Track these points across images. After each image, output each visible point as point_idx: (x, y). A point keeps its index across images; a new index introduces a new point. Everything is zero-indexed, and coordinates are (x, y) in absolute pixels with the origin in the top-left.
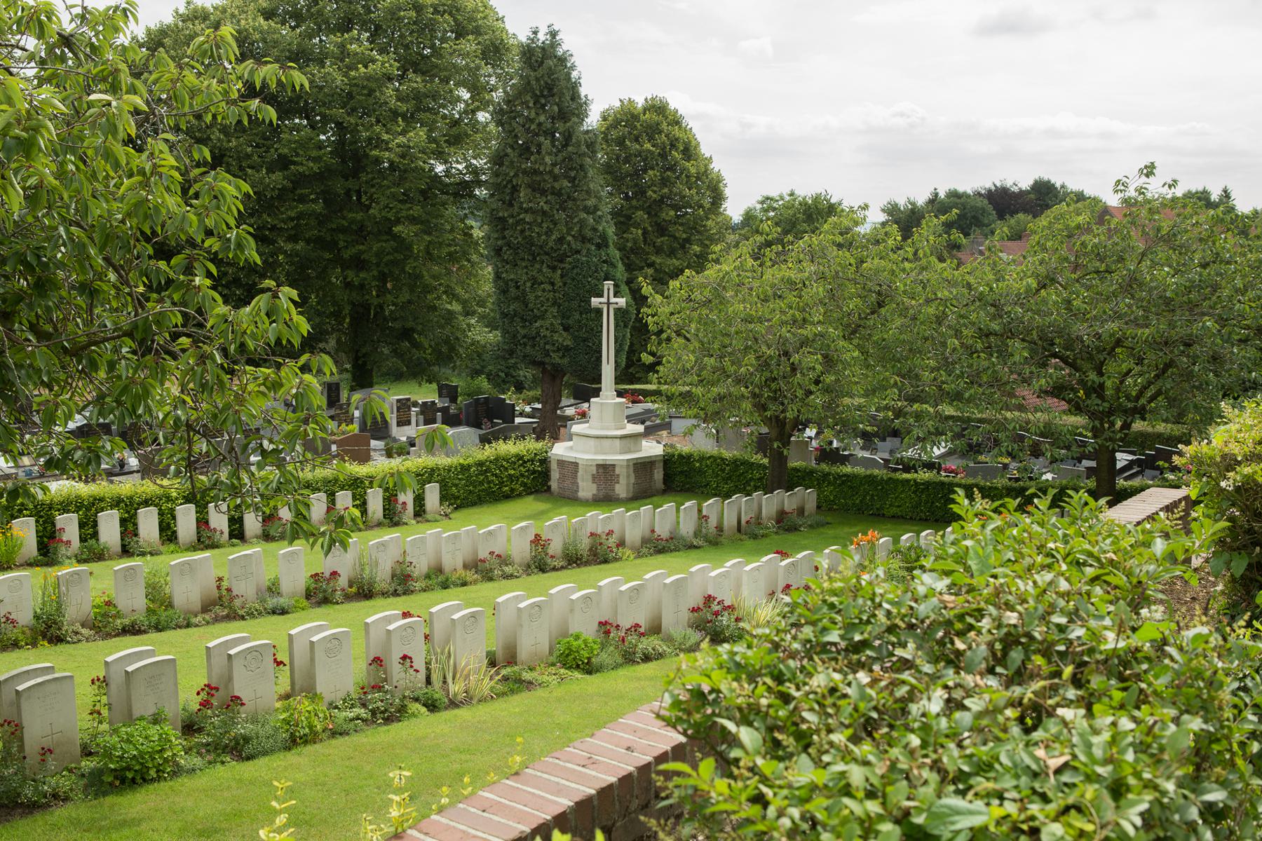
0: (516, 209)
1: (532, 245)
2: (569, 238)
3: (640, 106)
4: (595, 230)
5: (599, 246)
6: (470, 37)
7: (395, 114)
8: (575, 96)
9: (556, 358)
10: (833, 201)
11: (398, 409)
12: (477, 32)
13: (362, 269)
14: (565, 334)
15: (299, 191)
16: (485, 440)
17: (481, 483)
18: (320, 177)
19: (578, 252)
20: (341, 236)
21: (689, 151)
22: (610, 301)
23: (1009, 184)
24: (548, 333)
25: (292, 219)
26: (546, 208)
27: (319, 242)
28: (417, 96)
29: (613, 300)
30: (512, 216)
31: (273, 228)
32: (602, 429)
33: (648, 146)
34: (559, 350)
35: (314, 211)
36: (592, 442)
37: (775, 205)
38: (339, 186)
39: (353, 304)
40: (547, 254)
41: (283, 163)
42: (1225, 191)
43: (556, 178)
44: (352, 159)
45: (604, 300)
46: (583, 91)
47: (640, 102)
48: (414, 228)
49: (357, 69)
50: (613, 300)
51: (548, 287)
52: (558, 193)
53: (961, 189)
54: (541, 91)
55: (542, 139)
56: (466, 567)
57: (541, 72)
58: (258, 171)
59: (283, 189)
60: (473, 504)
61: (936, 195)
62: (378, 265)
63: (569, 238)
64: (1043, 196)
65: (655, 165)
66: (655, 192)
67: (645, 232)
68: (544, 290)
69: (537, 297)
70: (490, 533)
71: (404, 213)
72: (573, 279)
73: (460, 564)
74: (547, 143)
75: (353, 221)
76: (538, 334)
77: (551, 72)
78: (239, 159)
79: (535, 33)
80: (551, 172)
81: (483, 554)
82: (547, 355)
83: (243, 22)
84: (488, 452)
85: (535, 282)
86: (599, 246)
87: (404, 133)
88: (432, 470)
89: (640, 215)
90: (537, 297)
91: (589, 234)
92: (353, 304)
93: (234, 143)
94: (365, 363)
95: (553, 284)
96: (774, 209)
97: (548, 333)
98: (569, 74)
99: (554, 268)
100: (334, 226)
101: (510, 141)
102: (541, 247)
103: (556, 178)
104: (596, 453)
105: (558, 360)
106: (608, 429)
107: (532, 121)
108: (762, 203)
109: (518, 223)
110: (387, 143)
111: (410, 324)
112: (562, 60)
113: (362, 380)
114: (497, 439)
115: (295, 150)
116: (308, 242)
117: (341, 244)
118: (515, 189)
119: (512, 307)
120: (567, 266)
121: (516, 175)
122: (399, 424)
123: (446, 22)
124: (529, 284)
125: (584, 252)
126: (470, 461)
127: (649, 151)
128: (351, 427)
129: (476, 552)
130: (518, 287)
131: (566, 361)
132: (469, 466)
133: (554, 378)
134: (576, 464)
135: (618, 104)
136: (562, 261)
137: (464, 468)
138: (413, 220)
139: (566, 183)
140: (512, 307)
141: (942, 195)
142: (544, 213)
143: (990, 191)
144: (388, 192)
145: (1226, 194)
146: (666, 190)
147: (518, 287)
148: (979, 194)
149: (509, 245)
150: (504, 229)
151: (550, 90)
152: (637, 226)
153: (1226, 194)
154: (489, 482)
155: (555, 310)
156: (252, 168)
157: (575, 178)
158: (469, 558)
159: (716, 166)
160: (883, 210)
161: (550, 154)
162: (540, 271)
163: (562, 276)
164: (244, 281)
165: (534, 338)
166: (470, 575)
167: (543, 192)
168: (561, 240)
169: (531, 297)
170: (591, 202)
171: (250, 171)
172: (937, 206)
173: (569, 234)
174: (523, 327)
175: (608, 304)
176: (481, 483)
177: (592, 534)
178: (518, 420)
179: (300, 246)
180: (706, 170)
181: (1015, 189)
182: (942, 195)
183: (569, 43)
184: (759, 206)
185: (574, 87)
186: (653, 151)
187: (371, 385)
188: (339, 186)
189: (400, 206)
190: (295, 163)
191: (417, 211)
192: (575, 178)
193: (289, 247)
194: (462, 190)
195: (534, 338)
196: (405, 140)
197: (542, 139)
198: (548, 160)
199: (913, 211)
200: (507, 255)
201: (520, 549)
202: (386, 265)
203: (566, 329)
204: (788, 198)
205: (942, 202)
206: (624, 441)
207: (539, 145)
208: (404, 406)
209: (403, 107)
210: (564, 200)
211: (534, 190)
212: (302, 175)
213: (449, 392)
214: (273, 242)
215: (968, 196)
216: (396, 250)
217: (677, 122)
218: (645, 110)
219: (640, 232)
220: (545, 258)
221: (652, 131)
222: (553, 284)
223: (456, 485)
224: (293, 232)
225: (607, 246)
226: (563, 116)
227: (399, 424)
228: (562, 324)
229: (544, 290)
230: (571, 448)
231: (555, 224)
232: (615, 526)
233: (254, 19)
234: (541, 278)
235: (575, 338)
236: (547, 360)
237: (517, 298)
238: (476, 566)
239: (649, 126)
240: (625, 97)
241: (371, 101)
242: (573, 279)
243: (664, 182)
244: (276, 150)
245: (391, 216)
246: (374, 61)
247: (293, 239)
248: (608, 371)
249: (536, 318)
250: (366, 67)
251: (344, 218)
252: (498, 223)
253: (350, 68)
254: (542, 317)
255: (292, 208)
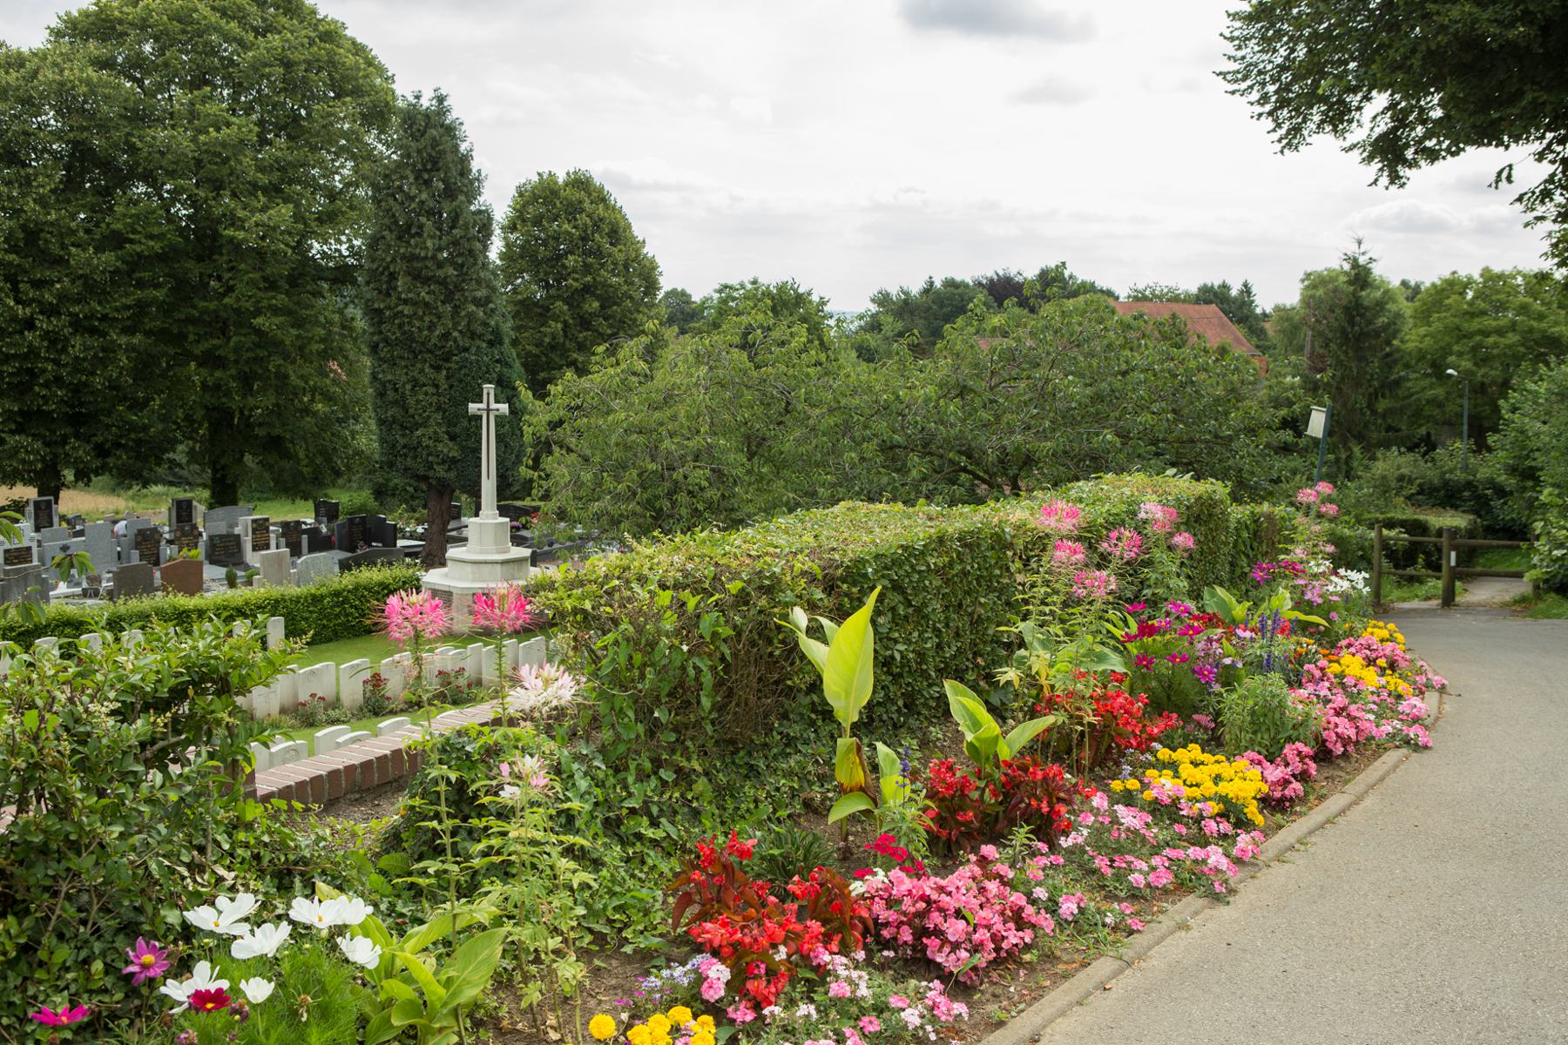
0: (394, 300)
1: (413, 340)
2: (455, 334)
3: (561, 181)
4: (486, 324)
5: (491, 344)
6: (348, 99)
7: (255, 186)
8: (464, 170)
9: (441, 471)
10: (801, 291)
11: (254, 530)
12: (357, 92)
13: (218, 368)
14: (451, 444)
15: (137, 275)
16: (345, 566)
17: (337, 616)
18: (162, 258)
19: (466, 350)
20: (191, 328)
21: (617, 231)
22: (489, 407)
23: (1012, 272)
24: (431, 443)
25: (128, 307)
26: (427, 298)
27: (163, 335)
28: (282, 167)
29: (494, 406)
30: (389, 308)
31: (104, 318)
32: (481, 552)
33: (566, 226)
34: (444, 462)
35: (155, 299)
36: (469, 568)
37: (735, 294)
38: (193, 269)
39: (206, 407)
40: (430, 351)
41: (116, 241)
42: (1245, 285)
43: (440, 265)
44: (206, 239)
45: (483, 406)
46: (475, 166)
47: (561, 178)
48: (277, 320)
49: (208, 133)
50: (494, 406)
51: (431, 390)
52: (443, 282)
53: (958, 279)
54: (424, 165)
55: (423, 219)
56: (283, 711)
57: (423, 142)
58: (84, 250)
59: (116, 272)
60: (329, 640)
61: (932, 283)
62: (236, 362)
63: (455, 334)
64: (1053, 282)
65: (580, 253)
66: (576, 280)
67: (566, 325)
68: (426, 394)
69: (418, 401)
70: (312, 672)
71: (265, 303)
72: (461, 381)
73: (275, 710)
74: (429, 225)
75: (205, 311)
76: (419, 443)
77: (435, 143)
78: (61, 235)
79: (417, 97)
80: (434, 257)
81: (304, 697)
82: (431, 468)
83: (66, 73)
84: (348, 580)
85: (416, 384)
86: (491, 344)
87: (264, 210)
88: (277, 601)
89: (560, 305)
90: (418, 401)
91: (479, 330)
92: (206, 407)
93: (53, 216)
94: (224, 477)
95: (437, 386)
96: (734, 299)
97: (431, 443)
98: (456, 147)
99: (438, 368)
100: (182, 316)
101: (386, 221)
102: (423, 344)
103: (440, 265)
104: (473, 581)
105: (442, 474)
106: (488, 553)
107: (412, 199)
108: (720, 291)
109: (396, 315)
110: (243, 221)
111: (277, 431)
112: (450, 131)
113: (224, 495)
114: (359, 566)
115: (131, 226)
116: (148, 333)
117: (191, 337)
118: (393, 276)
119: (389, 413)
120: (453, 366)
121: (393, 260)
122: (256, 548)
123: (320, 81)
124: (408, 387)
125: (473, 350)
126: (324, 590)
127: (568, 233)
128: (194, 552)
129: (296, 695)
130: (396, 390)
131: (452, 475)
132: (323, 597)
133: (441, 494)
134: (450, 594)
135: (536, 178)
136: (447, 360)
137: (316, 599)
138: (276, 311)
139: (451, 271)
140: (389, 413)
141: (938, 284)
142: (427, 305)
143: (992, 280)
144: (245, 278)
145: (1247, 290)
146: (589, 278)
147: (396, 390)
148: (980, 284)
149: (386, 341)
150: (381, 322)
151: (435, 163)
152: (556, 318)
153: (1247, 290)
154: (347, 615)
155: (439, 416)
156: (78, 246)
157: (462, 266)
158: (288, 701)
159: (649, 250)
160: (873, 301)
161: (432, 237)
162: (422, 371)
163: (448, 378)
164: (67, 379)
165: (415, 449)
166: (288, 720)
167: (427, 281)
168: (446, 336)
169: (411, 401)
170: (481, 293)
171: (73, 250)
172: (931, 296)
173: (455, 329)
174: (403, 435)
175: (488, 410)
176: (337, 616)
177: (440, 673)
178: (400, 543)
179: (137, 339)
180: (637, 256)
181: (1019, 279)
182: (938, 284)
183: (458, 111)
184: (716, 296)
185: (465, 160)
186: (575, 229)
187: (234, 502)
188: (193, 269)
189: (261, 294)
190: (132, 241)
191: (281, 300)
192: (462, 266)
193: (123, 340)
194: (342, 275)
195: (415, 449)
196: (265, 217)
197: (423, 219)
198: (429, 244)
199: (906, 302)
200: (384, 352)
201: (353, 692)
202: (247, 363)
203: (453, 438)
204: (749, 287)
205: (938, 293)
206: (506, 567)
207: (421, 226)
208: (261, 527)
209: (264, 179)
210: (450, 292)
211: (415, 278)
212: (140, 255)
213: (328, 511)
214: (104, 334)
215: (966, 286)
216: (257, 346)
217: (602, 198)
218: (566, 184)
219: (559, 326)
220: (427, 356)
221: (573, 210)
222: (437, 386)
223: (306, 619)
224: (129, 323)
225: (501, 343)
226: (450, 193)
227: (256, 548)
228: (447, 433)
229: (426, 394)
230: (446, 575)
231: (440, 318)
232: (470, 666)
233: (81, 70)
234: (423, 379)
235: (463, 449)
236: (431, 473)
237: (396, 402)
238: (296, 711)
239: (570, 204)
240: (545, 170)
241: (225, 171)
242: (461, 381)
243: (587, 269)
244: (108, 225)
245: (249, 305)
246: (228, 125)
247: (129, 331)
248: (488, 486)
249: (417, 426)
250: (218, 130)
251: (194, 307)
252: (375, 315)
253: (200, 131)
254: (424, 425)
255: (127, 295)
